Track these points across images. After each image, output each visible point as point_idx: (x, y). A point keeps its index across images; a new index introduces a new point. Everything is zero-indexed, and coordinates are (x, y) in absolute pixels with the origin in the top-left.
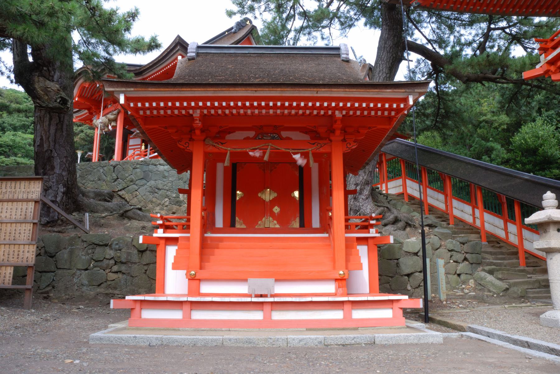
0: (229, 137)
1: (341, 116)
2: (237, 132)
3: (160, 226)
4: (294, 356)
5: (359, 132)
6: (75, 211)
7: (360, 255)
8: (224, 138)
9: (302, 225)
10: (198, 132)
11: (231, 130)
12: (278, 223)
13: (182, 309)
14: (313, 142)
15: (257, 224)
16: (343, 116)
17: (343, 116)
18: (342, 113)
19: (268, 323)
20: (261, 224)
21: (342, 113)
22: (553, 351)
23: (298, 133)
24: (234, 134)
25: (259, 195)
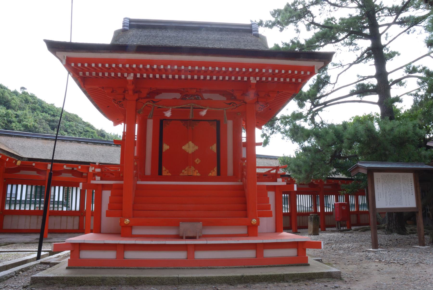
0: (158, 97)
1: (255, 82)
2: (163, 94)
3: (98, 174)
4: (359, 276)
5: (270, 96)
6: (326, 64)
7: (268, 196)
8: (154, 98)
9: (219, 173)
10: (131, 92)
11: (158, 92)
12: (199, 172)
13: (116, 250)
14: (230, 102)
15: (181, 172)
16: (257, 81)
17: (257, 81)
18: (256, 79)
19: (121, 264)
20: (185, 173)
21: (256, 79)
22: (187, 281)
23: (218, 95)
24: (161, 95)
25: (184, 148)
